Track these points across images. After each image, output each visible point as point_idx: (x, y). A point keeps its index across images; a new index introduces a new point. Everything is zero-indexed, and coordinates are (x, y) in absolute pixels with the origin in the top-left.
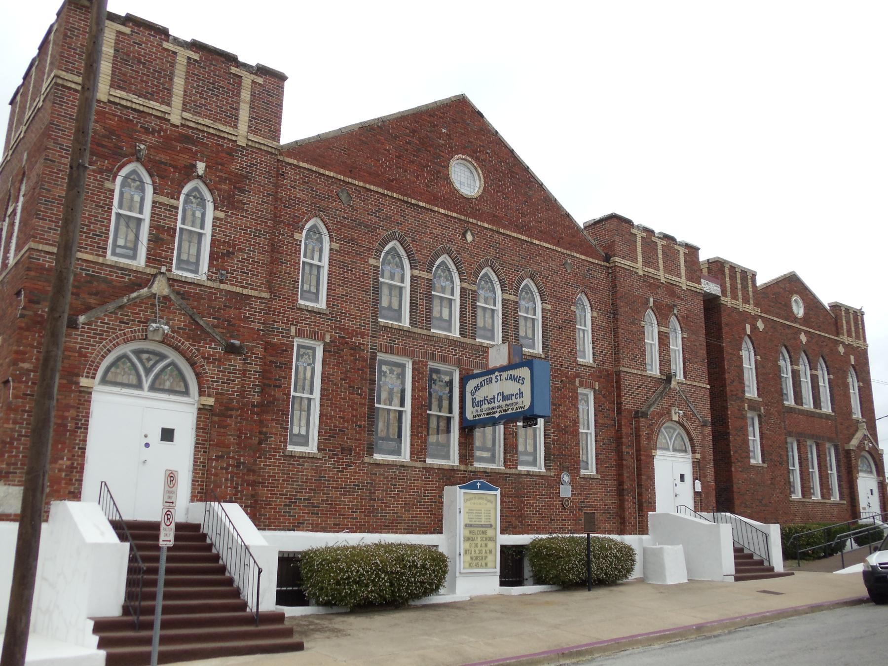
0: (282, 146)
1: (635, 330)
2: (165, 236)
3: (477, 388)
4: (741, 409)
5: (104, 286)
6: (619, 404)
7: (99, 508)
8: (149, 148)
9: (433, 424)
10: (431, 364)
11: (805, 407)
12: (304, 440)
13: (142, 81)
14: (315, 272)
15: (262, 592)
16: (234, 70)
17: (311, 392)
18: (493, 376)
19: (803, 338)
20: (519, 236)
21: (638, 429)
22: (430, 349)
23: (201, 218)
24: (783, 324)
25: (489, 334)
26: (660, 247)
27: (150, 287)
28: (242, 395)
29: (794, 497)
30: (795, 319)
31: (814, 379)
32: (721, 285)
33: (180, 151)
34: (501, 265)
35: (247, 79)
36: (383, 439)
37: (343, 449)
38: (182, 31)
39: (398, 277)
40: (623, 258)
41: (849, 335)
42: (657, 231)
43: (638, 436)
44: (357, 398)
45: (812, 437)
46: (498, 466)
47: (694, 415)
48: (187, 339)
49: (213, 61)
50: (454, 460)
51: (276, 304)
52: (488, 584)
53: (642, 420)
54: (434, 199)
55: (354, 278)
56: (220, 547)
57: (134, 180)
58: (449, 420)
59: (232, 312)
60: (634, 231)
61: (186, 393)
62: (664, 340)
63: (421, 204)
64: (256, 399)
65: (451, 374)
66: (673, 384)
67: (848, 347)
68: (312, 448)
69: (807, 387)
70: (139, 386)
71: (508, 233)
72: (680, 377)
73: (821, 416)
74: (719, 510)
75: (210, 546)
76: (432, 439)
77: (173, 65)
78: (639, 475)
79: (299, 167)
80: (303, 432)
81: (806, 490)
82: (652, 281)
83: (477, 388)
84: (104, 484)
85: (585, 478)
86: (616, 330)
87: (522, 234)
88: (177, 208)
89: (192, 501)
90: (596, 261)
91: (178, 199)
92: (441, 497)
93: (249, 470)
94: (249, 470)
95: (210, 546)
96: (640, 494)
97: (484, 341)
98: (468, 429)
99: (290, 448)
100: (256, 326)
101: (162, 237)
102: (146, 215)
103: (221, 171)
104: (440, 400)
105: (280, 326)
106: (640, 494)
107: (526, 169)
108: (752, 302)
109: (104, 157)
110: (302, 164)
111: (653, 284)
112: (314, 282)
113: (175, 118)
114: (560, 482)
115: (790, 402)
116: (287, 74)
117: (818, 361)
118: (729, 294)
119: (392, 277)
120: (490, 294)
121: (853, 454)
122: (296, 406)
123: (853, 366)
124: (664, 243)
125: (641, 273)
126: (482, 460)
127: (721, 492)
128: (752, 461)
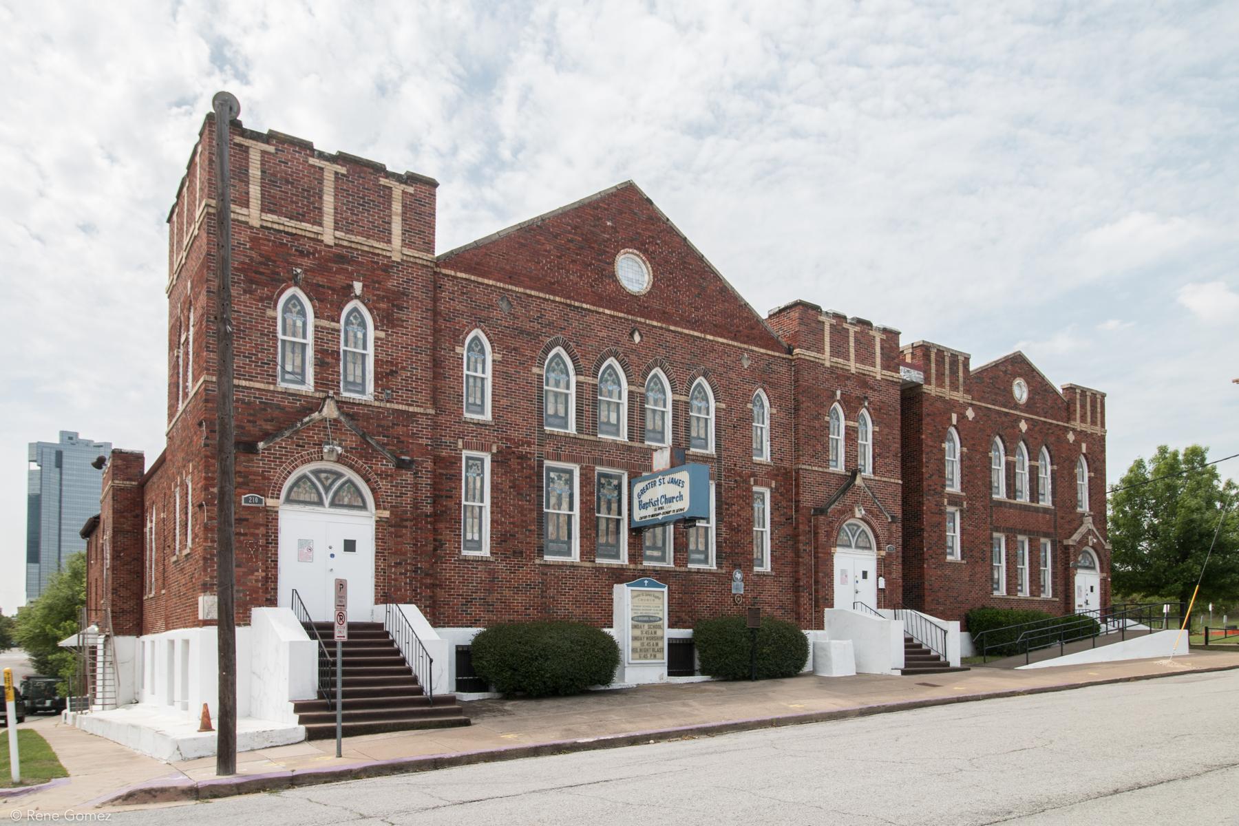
0: (438, 258)
1: (817, 426)
2: (330, 360)
3: (643, 491)
4: (939, 505)
5: (277, 413)
7: (292, 613)
8: (305, 271)
9: (603, 526)
10: (599, 469)
12: (478, 545)
13: (292, 202)
14: (479, 383)
15: (440, 678)
16: (383, 181)
17: (482, 501)
19: (1023, 426)
20: (692, 332)
21: (816, 527)
22: (597, 454)
23: (363, 337)
24: (998, 412)
25: (659, 436)
26: (852, 334)
27: (320, 411)
28: (416, 506)
29: (996, 593)
30: (1016, 406)
31: (1034, 472)
32: (925, 372)
33: (336, 273)
34: (671, 364)
35: (398, 189)
36: (552, 541)
37: (514, 552)
38: (325, 143)
39: (562, 384)
40: (808, 349)
43: (816, 534)
44: (526, 505)
45: (1024, 532)
46: (669, 564)
47: (881, 512)
48: (361, 457)
49: (361, 173)
50: (624, 560)
51: (442, 419)
52: (655, 672)
53: (821, 518)
54: (600, 300)
55: (519, 390)
56: (401, 642)
57: (294, 306)
58: (618, 521)
59: (400, 430)
60: (822, 318)
61: (364, 507)
62: (851, 435)
63: (585, 306)
65: (619, 478)
66: (858, 481)
67: (1081, 435)
68: (486, 552)
70: (320, 503)
71: (679, 329)
72: (868, 472)
74: (905, 606)
75: (392, 642)
76: (602, 540)
77: (321, 181)
79: (456, 278)
80: (476, 537)
82: (840, 372)
83: (643, 491)
84: (295, 591)
85: (759, 575)
87: (694, 329)
88: (339, 331)
89: (376, 603)
90: (777, 354)
91: (338, 322)
92: (611, 594)
93: (427, 575)
94: (427, 575)
95: (392, 642)
96: (817, 591)
98: (637, 532)
99: (464, 553)
100: (424, 441)
101: (327, 359)
102: (310, 340)
103: (378, 289)
104: (609, 503)
105: (447, 439)
106: (817, 591)
107: (701, 258)
108: (961, 389)
109: (265, 285)
110: (459, 275)
111: (841, 376)
112: (479, 395)
114: (731, 578)
115: (1001, 495)
116: (438, 180)
117: (1040, 450)
118: (933, 381)
119: (557, 384)
120: (660, 396)
121: (1072, 550)
122: (468, 514)
124: (857, 329)
125: (827, 364)
126: (651, 558)
127: (908, 587)
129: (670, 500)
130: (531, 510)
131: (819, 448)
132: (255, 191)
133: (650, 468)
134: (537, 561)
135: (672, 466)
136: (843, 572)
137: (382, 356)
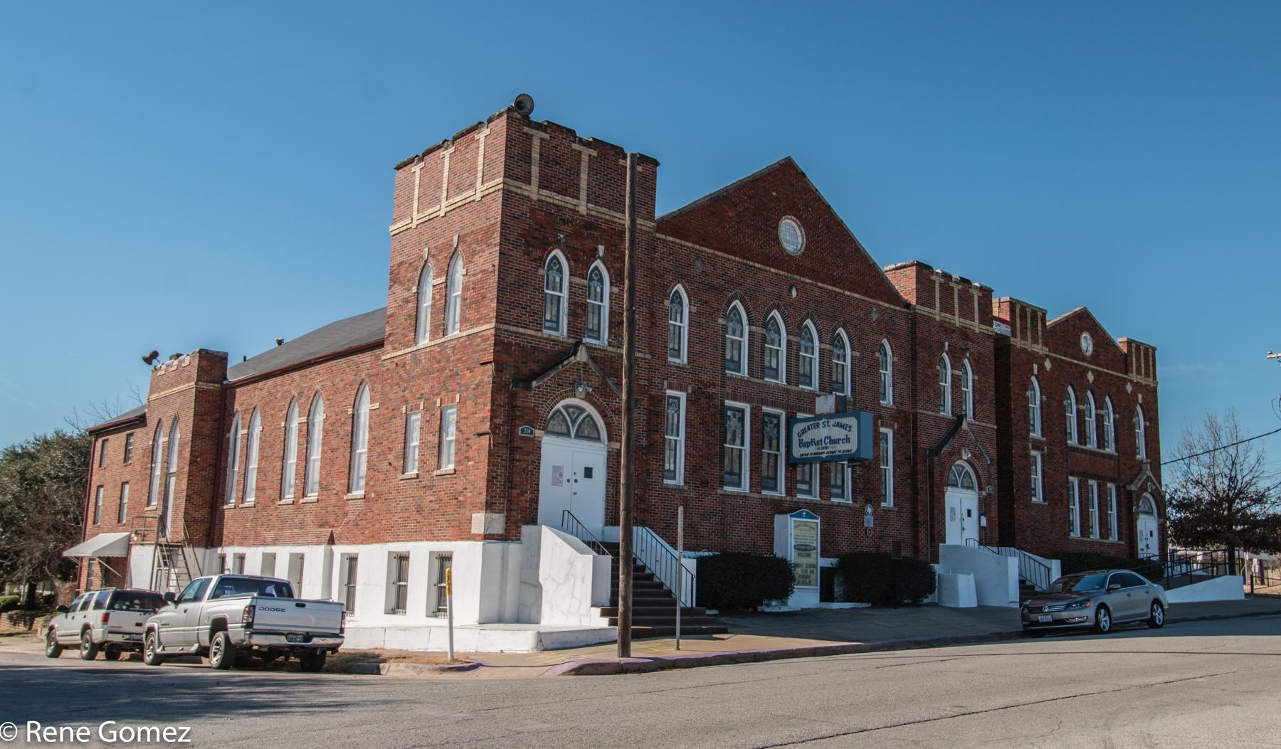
2: (579, 311)
3: (804, 431)
4: (1026, 449)
6: (915, 443)
10: (765, 409)
11: (1089, 447)
19: (1090, 377)
21: (931, 468)
24: (1070, 364)
26: (956, 292)
30: (1083, 358)
31: (1100, 419)
41: (1139, 372)
42: (955, 276)
50: (781, 492)
55: (708, 336)
60: (933, 277)
61: (598, 439)
64: (644, 442)
66: (964, 426)
67: (1137, 386)
69: (1090, 422)
70: (568, 435)
73: (1103, 456)
77: (579, 164)
78: (932, 509)
81: (1085, 529)
83: (804, 431)
86: (914, 373)
99: (666, 481)
101: (579, 310)
104: (771, 440)
107: (840, 224)
111: (947, 329)
113: (582, 210)
114: (864, 513)
115: (1073, 441)
124: (960, 287)
125: (938, 318)
128: (1034, 499)
129: (836, 441)
132: (535, 170)
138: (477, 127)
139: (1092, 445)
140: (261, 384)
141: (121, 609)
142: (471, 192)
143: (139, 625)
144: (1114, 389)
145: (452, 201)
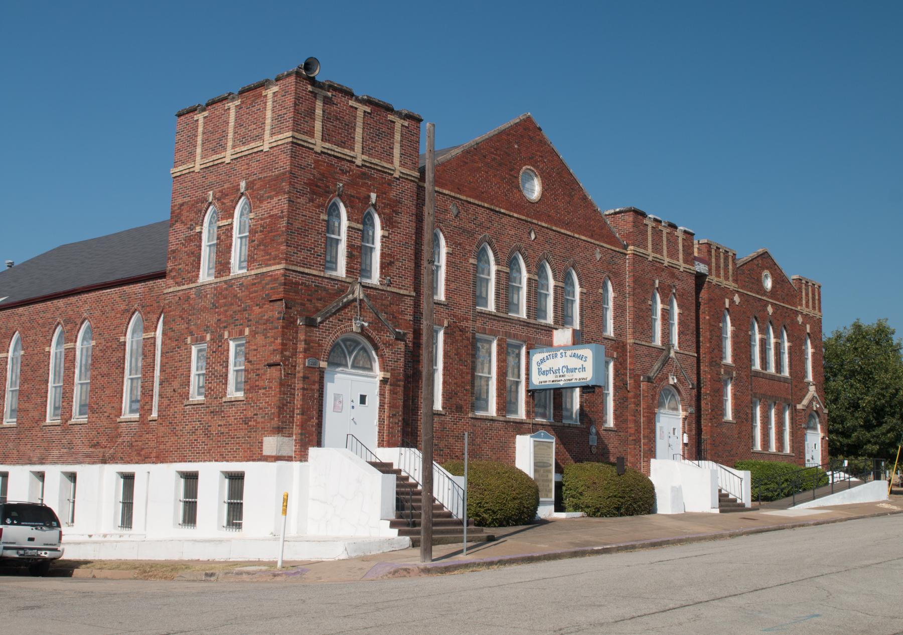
2: (355, 253)
3: (543, 361)
18: (559, 353)
19: (770, 309)
31: (778, 347)
48: (374, 330)
55: (466, 280)
60: (646, 221)
66: (672, 354)
67: (805, 316)
83: (543, 361)
97: (425, 304)
108: (731, 279)
114: (589, 433)
115: (757, 366)
123: (727, 309)
129: (573, 370)
130: (468, 373)
131: (645, 326)
132: (318, 125)
133: (550, 344)
134: (470, 415)
135: (574, 344)
136: (337, 397)
137: (385, 250)
138: (264, 84)
139: (772, 369)
140: (21, 309)
141: (12, 524)
142: (258, 143)
143: (31, 539)
144: (788, 321)
145: (238, 150)
